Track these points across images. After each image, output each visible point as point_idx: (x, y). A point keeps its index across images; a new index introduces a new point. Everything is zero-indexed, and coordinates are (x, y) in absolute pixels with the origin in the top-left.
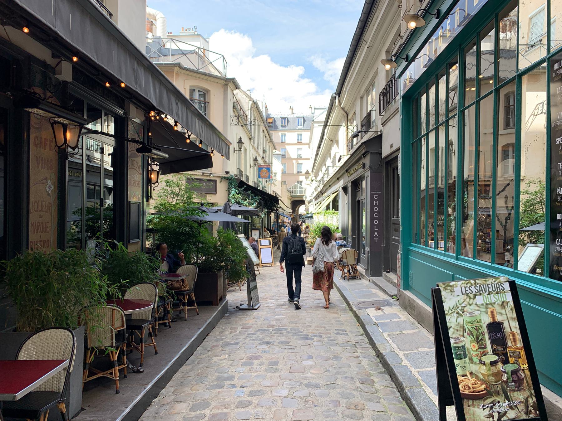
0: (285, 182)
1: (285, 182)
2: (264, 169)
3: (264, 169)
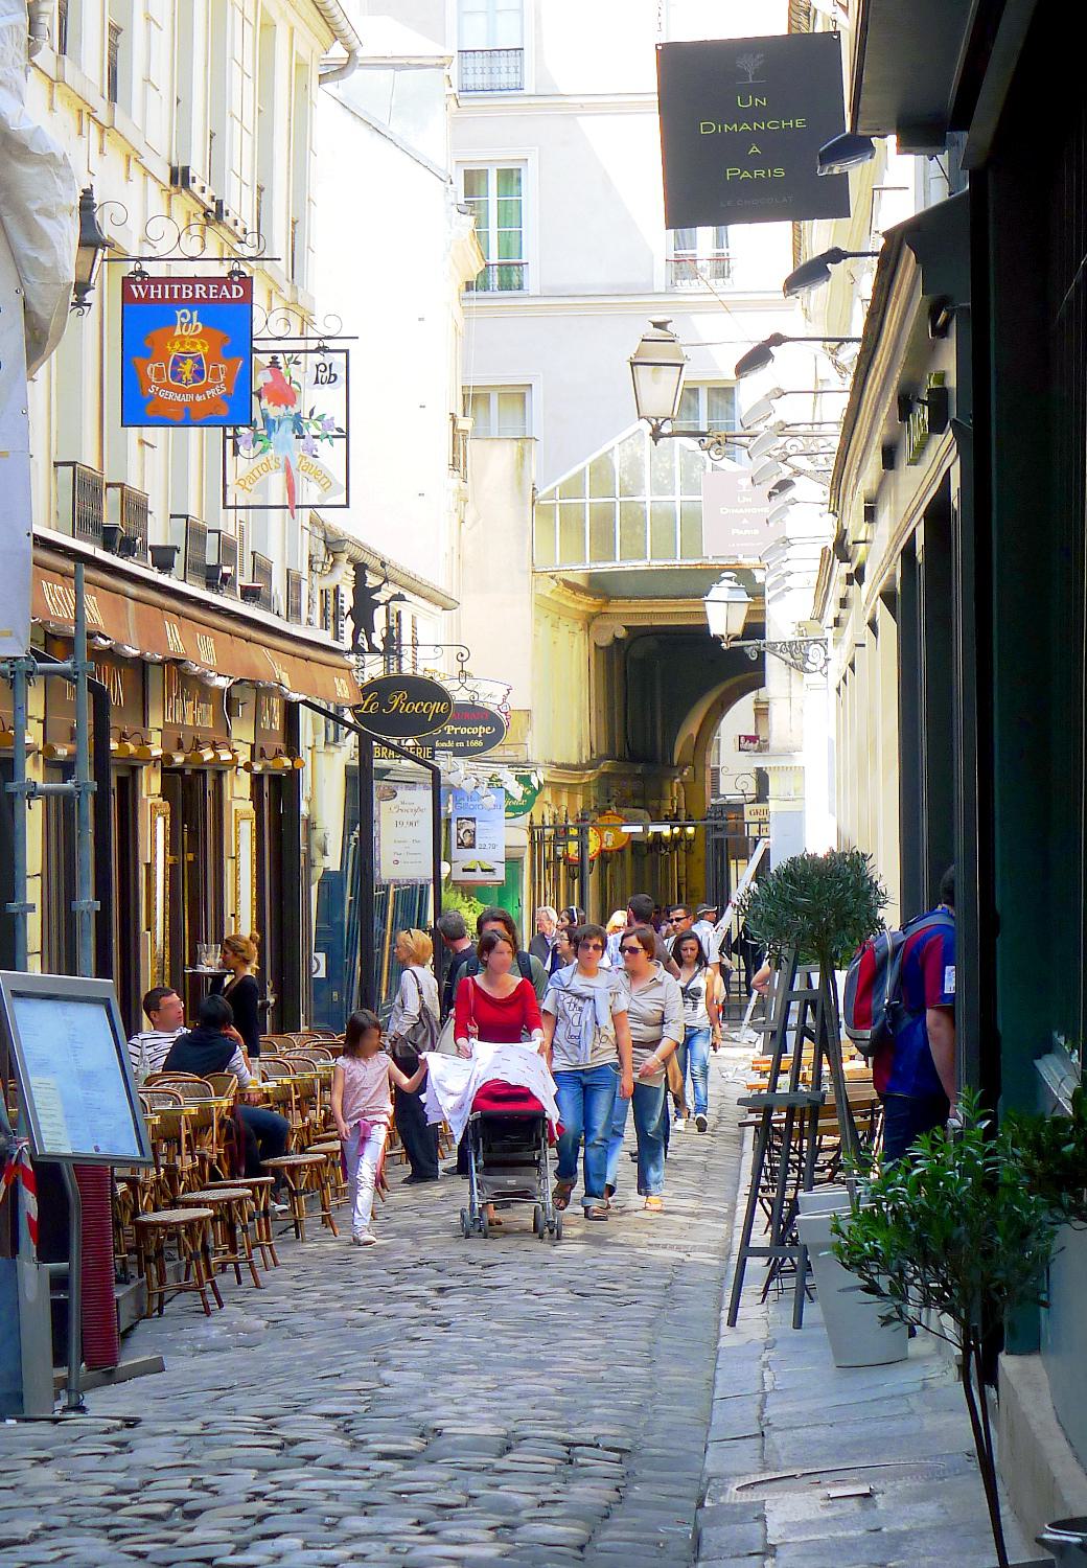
0: (518, 395)
1: (518, 395)
2: (188, 326)
3: (188, 326)
